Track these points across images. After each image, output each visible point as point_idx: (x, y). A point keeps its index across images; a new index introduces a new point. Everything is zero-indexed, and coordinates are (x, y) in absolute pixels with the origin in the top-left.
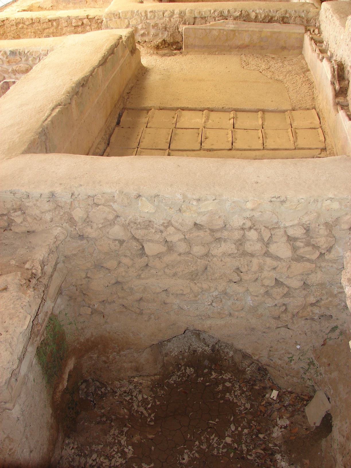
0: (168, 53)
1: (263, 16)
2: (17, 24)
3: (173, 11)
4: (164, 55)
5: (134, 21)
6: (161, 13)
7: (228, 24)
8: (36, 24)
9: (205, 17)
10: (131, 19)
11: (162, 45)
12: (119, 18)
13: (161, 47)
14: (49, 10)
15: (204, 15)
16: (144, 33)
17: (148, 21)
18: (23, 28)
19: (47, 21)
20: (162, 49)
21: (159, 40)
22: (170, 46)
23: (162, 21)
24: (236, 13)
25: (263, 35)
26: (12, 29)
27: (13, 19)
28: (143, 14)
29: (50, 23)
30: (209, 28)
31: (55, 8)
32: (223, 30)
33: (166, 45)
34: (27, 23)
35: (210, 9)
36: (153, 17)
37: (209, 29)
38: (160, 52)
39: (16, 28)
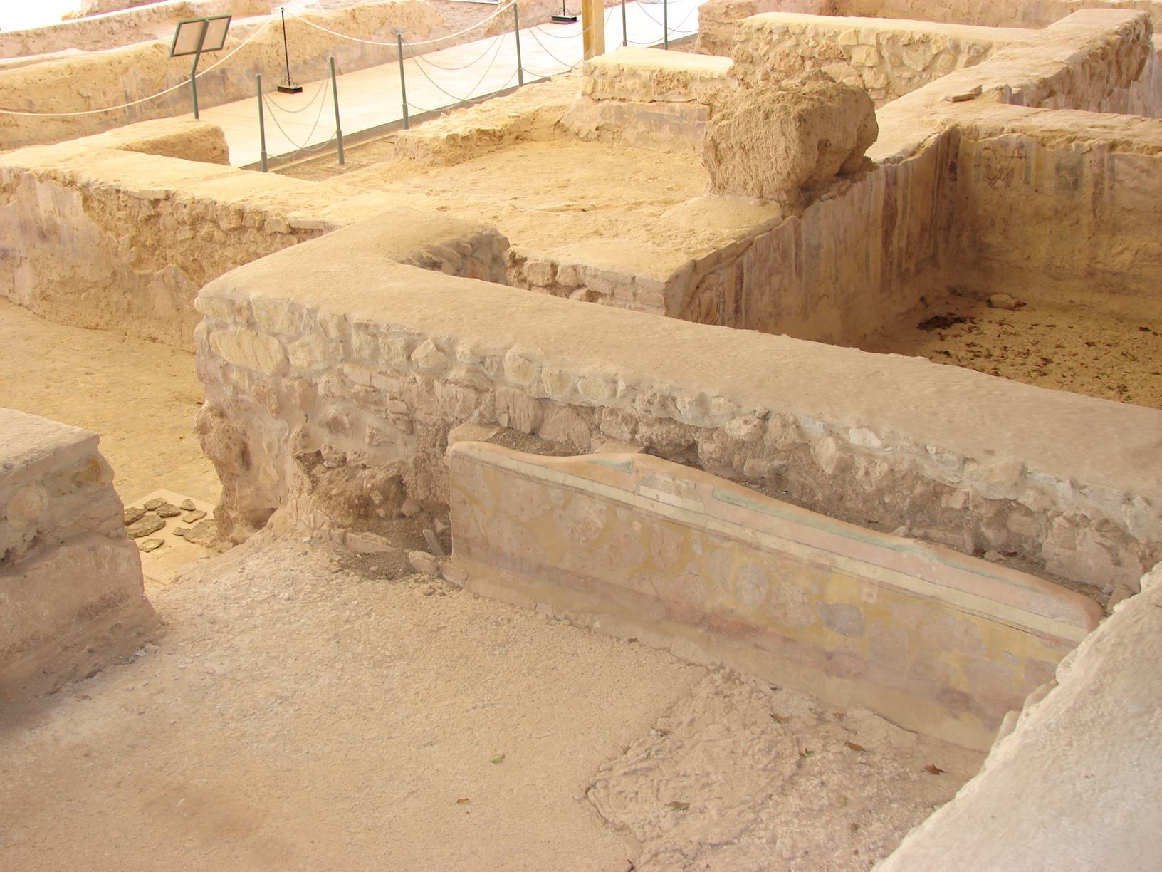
1: (881, 468)
2: (196, 222)
3: (452, 342)
4: (362, 565)
5: (300, 354)
6: (399, 344)
7: (649, 482)
8: (251, 235)
9: (593, 409)
10: (291, 340)
11: (386, 499)
12: (251, 324)
13: (381, 512)
14: (587, 139)
15: (582, 399)
16: (335, 419)
17: (347, 369)
18: (210, 239)
19: (283, 229)
21: (372, 478)
22: (423, 516)
23: (394, 384)
24: (737, 422)
25: (835, 593)
26: (180, 237)
28: (333, 332)
30: (560, 478)
31: (610, 135)
32: (628, 507)
33: (405, 509)
34: (224, 225)
35: (611, 369)
36: (366, 353)
37: (563, 486)
39: (189, 234)
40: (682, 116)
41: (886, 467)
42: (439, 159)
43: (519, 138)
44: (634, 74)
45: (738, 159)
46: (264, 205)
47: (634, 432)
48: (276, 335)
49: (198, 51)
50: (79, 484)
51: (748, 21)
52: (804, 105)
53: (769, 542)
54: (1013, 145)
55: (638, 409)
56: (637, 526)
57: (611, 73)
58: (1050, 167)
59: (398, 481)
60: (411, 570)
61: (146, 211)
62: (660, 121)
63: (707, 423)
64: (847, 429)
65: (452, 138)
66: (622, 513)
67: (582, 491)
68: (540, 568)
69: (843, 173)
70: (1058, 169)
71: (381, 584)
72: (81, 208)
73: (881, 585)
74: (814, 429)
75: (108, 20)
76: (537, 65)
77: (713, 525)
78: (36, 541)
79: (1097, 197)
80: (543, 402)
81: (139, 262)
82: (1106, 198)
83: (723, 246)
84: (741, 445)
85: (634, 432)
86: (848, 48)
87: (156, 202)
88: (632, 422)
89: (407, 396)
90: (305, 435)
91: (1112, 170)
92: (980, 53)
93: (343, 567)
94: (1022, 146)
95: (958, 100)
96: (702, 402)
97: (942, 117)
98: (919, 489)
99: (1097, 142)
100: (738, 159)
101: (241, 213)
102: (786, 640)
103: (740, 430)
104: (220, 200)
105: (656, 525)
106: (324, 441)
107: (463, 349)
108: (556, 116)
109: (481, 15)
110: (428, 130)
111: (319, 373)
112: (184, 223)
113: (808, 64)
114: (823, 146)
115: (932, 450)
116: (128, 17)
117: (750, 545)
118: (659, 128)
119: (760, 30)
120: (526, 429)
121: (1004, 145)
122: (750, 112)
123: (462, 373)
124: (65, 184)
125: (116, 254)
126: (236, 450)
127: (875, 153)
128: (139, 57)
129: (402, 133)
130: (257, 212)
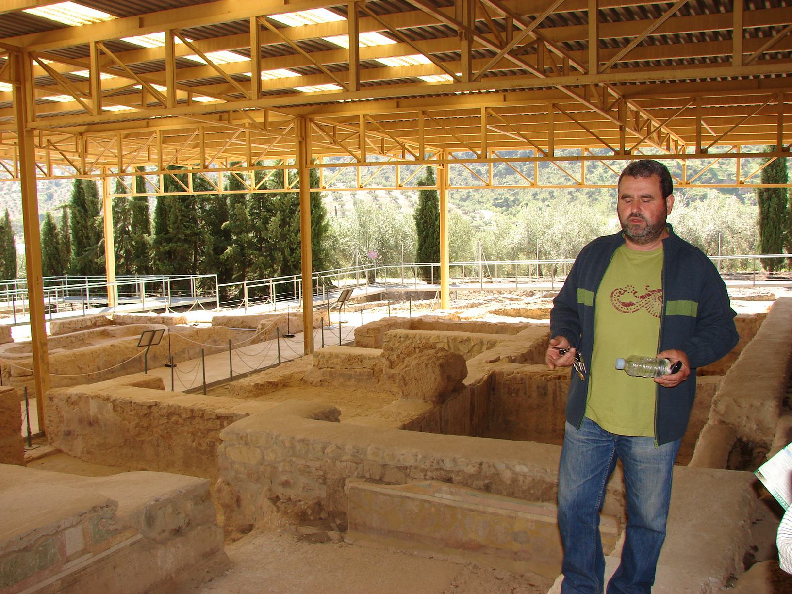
0: (313, 534)
1: (529, 480)
2: (170, 415)
4: (308, 538)
5: (271, 455)
7: (439, 491)
8: (197, 420)
9: (406, 468)
13: (312, 518)
14: (316, 386)
18: (176, 423)
19: (213, 417)
20: (311, 523)
24: (469, 467)
26: (161, 422)
27: (165, 405)
28: (288, 445)
29: (219, 422)
32: (430, 502)
34: (184, 416)
37: (401, 497)
38: (306, 530)
39: (166, 421)
40: (360, 374)
41: (531, 479)
42: (251, 394)
43: (285, 386)
44: (337, 356)
45: (414, 384)
46: (204, 407)
47: (425, 475)
48: (258, 447)
49: (149, 345)
50: (203, 501)
51: (389, 332)
52: (441, 361)
53: (490, 510)
54: (519, 378)
55: (427, 465)
56: (433, 509)
57: (327, 356)
58: (534, 387)
59: (319, 504)
60: (329, 539)
61: (145, 411)
62: (350, 377)
63: (457, 469)
64: (514, 466)
65: (257, 385)
66: (426, 505)
67: (409, 498)
68: (389, 532)
69: (454, 390)
70: (538, 388)
71: (319, 545)
72: (112, 411)
73: (536, 522)
74: (501, 467)
75: (71, 336)
76: (287, 354)
77: (466, 506)
78: (188, 524)
79: (554, 398)
80: (384, 466)
81: (139, 434)
82: (558, 399)
83: (414, 418)
84: (471, 476)
85: (425, 475)
86: (435, 343)
87: (150, 407)
88: (425, 471)
89: (323, 468)
90: (270, 490)
91: (560, 387)
92: (492, 345)
93: (299, 540)
94: (522, 379)
95: (491, 361)
96: (454, 460)
97: (487, 369)
98: (544, 486)
99: (553, 376)
100: (414, 384)
101: (192, 411)
102: (497, 549)
103: (471, 470)
104: (182, 405)
105: (442, 509)
106: (280, 491)
107: (349, 447)
108: (301, 376)
109: (245, 335)
110: (244, 381)
111: (279, 462)
112: (163, 416)
113: (417, 351)
114: (449, 377)
115: (549, 470)
116: (79, 335)
117: (482, 512)
118: (349, 380)
119: (395, 336)
120: (378, 478)
121: (515, 378)
122: (419, 364)
123: (349, 457)
124: (104, 400)
125: (128, 431)
126: (235, 499)
127: (467, 382)
128: (104, 350)
129: (232, 383)
130: (200, 410)
